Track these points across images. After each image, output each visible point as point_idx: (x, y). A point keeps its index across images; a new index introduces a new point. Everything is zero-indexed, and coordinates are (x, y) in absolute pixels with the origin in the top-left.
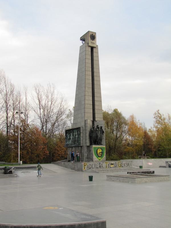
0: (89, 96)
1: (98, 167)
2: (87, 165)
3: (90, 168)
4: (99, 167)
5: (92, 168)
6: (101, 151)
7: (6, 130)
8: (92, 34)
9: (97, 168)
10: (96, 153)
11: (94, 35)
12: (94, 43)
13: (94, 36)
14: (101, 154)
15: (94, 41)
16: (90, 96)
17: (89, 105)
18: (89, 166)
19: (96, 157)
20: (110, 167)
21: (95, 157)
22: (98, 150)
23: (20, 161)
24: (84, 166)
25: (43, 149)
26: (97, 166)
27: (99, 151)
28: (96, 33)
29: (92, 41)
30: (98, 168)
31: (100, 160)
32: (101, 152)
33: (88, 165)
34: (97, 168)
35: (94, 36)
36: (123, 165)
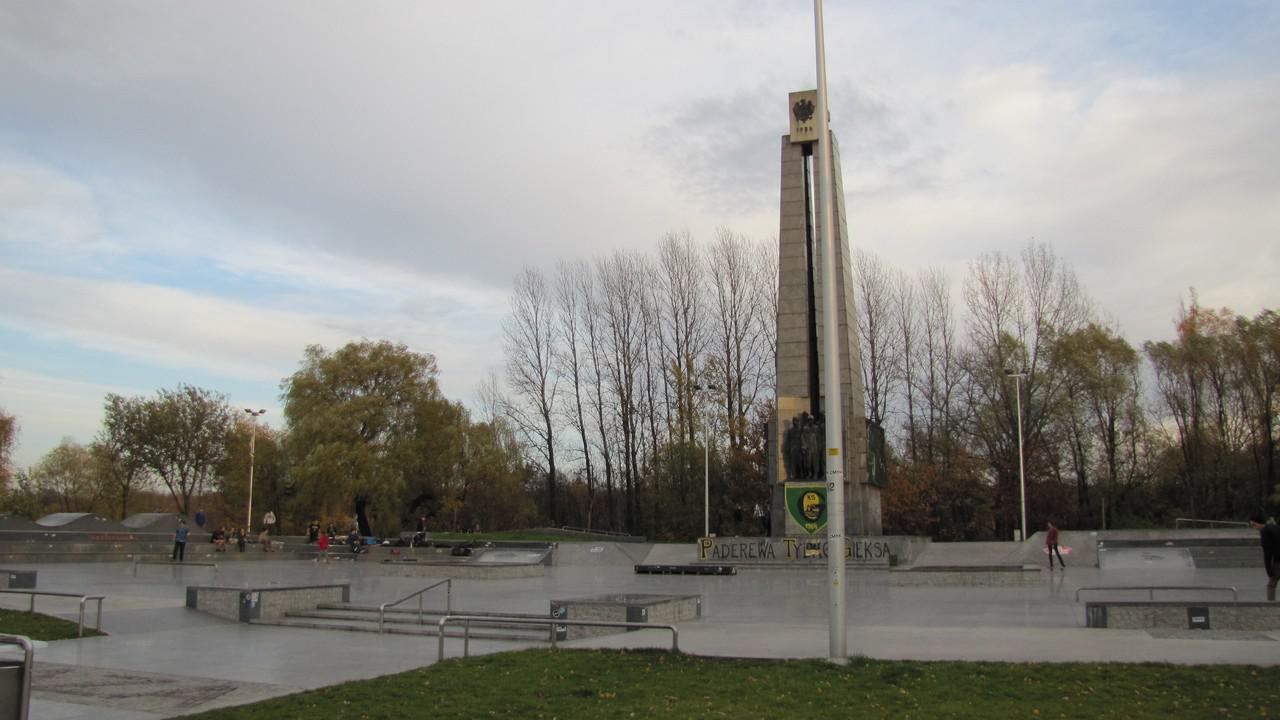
0: (793, 314)
1: (755, 552)
2: (713, 546)
3: (723, 557)
4: (757, 555)
5: (733, 556)
6: (816, 501)
7: (548, 466)
8: (803, 101)
9: (751, 557)
10: (796, 508)
11: (807, 101)
12: (811, 129)
13: (810, 102)
14: (817, 510)
15: (808, 123)
16: (796, 316)
17: (795, 344)
18: (720, 548)
19: (797, 523)
20: (805, 557)
21: (791, 521)
22: (806, 498)
23: (710, 532)
24: (704, 547)
25: (241, 537)
26: (751, 549)
27: (807, 502)
28: (790, 94)
29: (801, 122)
30: (754, 557)
31: (811, 531)
32: (816, 506)
33: (716, 547)
34: (751, 557)
35: (810, 102)
36: (862, 552)
